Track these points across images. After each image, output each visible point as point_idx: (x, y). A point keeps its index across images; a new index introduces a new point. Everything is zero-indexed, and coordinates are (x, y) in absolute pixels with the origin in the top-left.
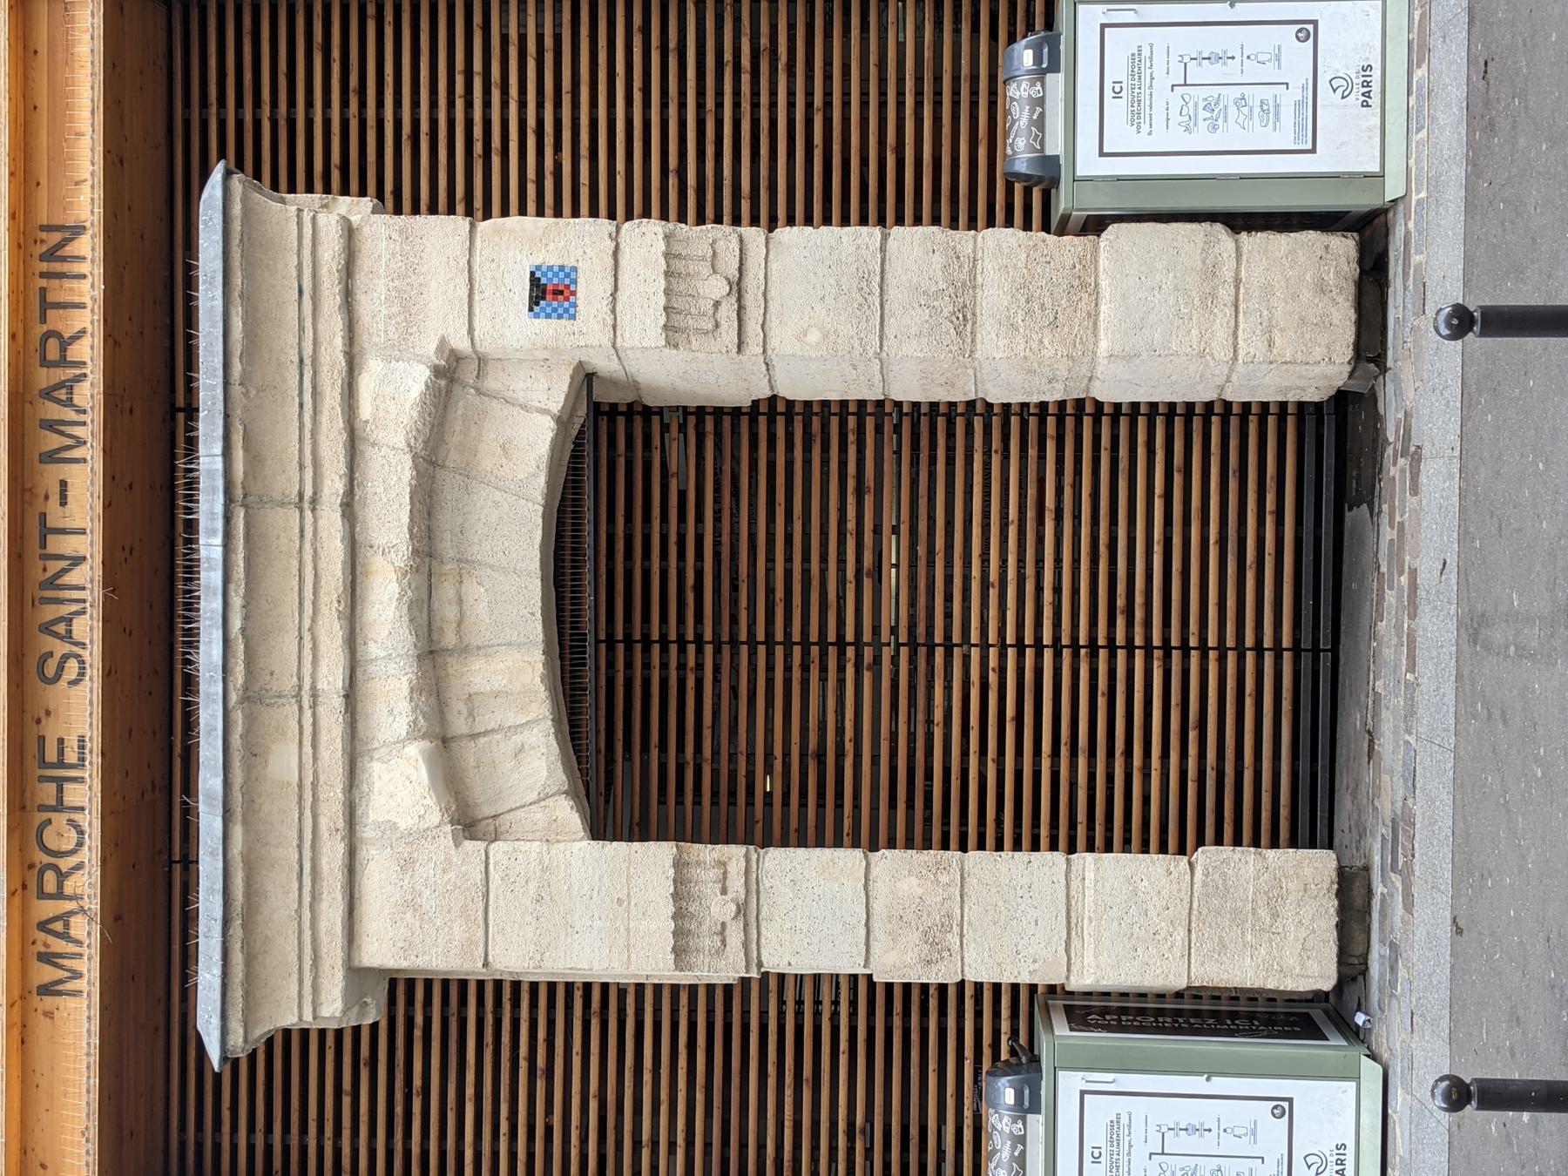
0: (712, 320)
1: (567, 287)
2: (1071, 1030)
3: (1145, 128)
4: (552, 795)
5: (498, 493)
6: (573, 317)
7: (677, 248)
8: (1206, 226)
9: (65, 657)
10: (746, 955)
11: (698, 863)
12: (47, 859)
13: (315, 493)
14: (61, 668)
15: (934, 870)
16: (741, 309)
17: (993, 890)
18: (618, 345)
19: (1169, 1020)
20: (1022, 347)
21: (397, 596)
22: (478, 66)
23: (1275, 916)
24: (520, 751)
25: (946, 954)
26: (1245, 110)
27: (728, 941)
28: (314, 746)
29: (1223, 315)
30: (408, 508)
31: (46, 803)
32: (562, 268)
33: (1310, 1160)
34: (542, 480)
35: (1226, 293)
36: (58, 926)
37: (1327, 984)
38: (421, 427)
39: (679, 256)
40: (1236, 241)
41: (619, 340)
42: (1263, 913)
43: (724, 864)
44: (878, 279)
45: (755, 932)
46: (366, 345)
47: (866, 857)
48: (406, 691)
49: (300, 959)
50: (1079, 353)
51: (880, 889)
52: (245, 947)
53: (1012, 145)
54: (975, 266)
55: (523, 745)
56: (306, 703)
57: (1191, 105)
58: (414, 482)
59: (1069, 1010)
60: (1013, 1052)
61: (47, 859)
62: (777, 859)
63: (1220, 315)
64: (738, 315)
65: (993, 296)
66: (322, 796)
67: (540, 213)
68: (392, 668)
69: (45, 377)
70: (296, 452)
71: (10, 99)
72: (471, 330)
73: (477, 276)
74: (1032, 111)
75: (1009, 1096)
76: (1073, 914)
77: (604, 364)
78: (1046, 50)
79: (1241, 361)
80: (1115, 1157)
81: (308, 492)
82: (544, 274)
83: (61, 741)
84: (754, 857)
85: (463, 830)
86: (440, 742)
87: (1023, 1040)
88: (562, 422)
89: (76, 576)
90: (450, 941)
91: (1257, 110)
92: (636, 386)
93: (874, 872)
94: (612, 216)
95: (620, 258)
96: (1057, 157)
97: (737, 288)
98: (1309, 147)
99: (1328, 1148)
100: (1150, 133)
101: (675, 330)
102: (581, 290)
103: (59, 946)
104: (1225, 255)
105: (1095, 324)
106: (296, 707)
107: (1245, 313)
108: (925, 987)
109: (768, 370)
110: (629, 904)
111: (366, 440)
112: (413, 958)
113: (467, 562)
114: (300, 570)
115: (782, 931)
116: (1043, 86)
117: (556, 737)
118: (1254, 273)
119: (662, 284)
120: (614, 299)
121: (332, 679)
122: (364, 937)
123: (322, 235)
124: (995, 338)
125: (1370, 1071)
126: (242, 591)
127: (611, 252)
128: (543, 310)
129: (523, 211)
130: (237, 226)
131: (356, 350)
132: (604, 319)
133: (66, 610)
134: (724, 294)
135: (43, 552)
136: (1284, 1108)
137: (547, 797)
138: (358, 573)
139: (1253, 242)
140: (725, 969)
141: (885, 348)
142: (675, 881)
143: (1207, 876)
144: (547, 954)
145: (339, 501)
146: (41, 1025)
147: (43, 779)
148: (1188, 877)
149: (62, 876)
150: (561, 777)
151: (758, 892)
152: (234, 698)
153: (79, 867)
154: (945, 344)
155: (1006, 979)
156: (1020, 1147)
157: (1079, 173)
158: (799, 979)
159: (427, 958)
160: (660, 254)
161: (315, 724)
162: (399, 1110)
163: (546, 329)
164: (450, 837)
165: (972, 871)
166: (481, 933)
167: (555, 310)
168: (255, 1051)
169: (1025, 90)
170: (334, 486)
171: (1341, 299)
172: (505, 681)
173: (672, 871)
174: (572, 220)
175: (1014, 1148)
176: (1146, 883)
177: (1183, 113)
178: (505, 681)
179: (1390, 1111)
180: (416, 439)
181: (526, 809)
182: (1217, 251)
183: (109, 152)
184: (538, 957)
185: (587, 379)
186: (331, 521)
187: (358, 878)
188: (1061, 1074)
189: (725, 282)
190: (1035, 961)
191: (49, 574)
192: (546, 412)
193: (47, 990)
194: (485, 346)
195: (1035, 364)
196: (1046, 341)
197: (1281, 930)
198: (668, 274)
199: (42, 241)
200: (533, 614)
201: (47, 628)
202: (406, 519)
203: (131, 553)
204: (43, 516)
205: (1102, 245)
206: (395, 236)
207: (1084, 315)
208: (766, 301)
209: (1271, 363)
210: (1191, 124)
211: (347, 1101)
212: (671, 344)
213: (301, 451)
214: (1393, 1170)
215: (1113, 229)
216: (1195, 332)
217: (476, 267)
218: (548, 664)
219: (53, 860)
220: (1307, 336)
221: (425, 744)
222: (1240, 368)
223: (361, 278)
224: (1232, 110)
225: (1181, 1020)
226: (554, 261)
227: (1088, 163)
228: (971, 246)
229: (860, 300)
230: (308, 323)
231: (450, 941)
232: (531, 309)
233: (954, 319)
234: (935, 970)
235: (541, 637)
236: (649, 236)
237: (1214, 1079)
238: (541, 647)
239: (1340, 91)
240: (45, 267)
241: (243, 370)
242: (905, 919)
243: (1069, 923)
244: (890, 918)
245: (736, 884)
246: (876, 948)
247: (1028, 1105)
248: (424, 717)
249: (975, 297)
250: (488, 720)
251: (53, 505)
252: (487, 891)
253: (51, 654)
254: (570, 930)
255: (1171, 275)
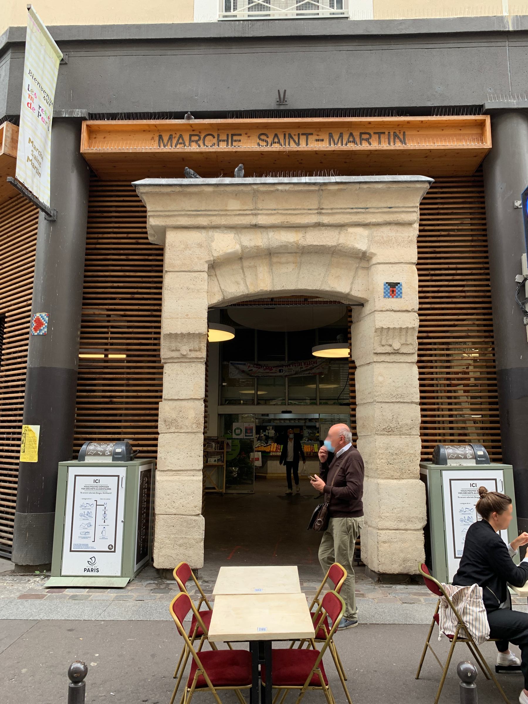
0: (385, 344)
1: (395, 295)
2: (141, 472)
3: (460, 495)
4: (223, 294)
5: (323, 275)
6: (385, 297)
7: (410, 332)
8: (426, 518)
9: (267, 142)
10: (169, 358)
11: (200, 342)
12: (202, 137)
13: (323, 213)
14: (263, 140)
15: (197, 422)
16: (389, 354)
17: (190, 444)
18: (376, 312)
19: (145, 506)
20: (380, 452)
21: (289, 241)
22: (459, 272)
23: (180, 546)
24: (238, 283)
25: (168, 427)
26: (86, 527)
27: (174, 352)
28: (239, 215)
29: (394, 525)
30: (318, 244)
31: (220, 137)
32: (401, 293)
33: (93, 559)
34: (328, 289)
35: (402, 525)
36: (181, 141)
37: (156, 565)
38: (346, 248)
39: (407, 332)
40: (421, 529)
41: (378, 313)
42: (181, 541)
43: (200, 350)
44: (402, 401)
45: (177, 361)
46: (373, 230)
47: (202, 399)
48: (257, 245)
49: (169, 211)
50: (379, 473)
51: (191, 404)
52: (173, 192)
53: (449, 448)
54: (407, 435)
55: (239, 284)
56: (253, 212)
57: (90, 507)
58: (327, 246)
59: (149, 471)
60: (135, 451)
61: (202, 137)
62: (203, 367)
63: (394, 523)
64: (387, 353)
65: (397, 442)
66: (222, 217)
67: (420, 286)
68: (265, 240)
69: (356, 134)
70: (337, 207)
71: (446, 121)
72: (379, 263)
73: (397, 265)
74: (462, 455)
75: (119, 450)
76: (181, 472)
77: (367, 309)
78: (484, 459)
79: (378, 531)
80: (96, 488)
81: (323, 211)
82: (399, 287)
83: (240, 141)
84: (202, 360)
85: (211, 264)
86: (241, 257)
87: (139, 455)
88: (347, 296)
89: (293, 144)
90: (174, 260)
91: (86, 531)
92: (359, 321)
93: (197, 402)
94: (420, 309)
95: (405, 312)
96: (447, 464)
97: (396, 352)
98: (72, 549)
99: (97, 566)
100: (459, 497)
101: (381, 332)
102: (394, 300)
103: (175, 141)
104: (415, 525)
105: (389, 478)
106: (252, 208)
107: (395, 533)
108: (157, 421)
109: (367, 364)
110: (187, 318)
111: (341, 230)
112: (169, 248)
113: (300, 265)
114: (297, 209)
115: (177, 370)
116: (471, 458)
117: (242, 295)
118: (409, 535)
119: (397, 326)
120: (391, 311)
121: (262, 220)
122: (176, 232)
123: (409, 214)
124: (383, 442)
125: (123, 582)
126: (291, 189)
127: (407, 309)
128: (387, 287)
129: (420, 281)
130: (412, 185)
131: (371, 226)
132: (384, 307)
133: (282, 141)
134: (394, 348)
135: (300, 134)
136: (112, 549)
137: (222, 292)
138: (297, 229)
139: (421, 536)
140: (164, 353)
141: (377, 404)
142: (194, 334)
143: (194, 521)
144: (169, 292)
145: (320, 221)
146: (150, 136)
147: (228, 135)
148: (194, 514)
149: (196, 142)
150: (229, 296)
151: (190, 362)
152: (255, 187)
153: (199, 146)
154: (380, 424)
155: (159, 449)
156: (101, 454)
157: (443, 472)
158: (161, 379)
159: (169, 252)
160: (407, 326)
161: (247, 215)
162: (122, 252)
163: (380, 288)
164: (209, 259)
165: (197, 436)
166: (177, 269)
167: (387, 291)
168: (139, 197)
169: (469, 452)
170: (326, 220)
171: (401, 568)
172: (261, 278)
173: (197, 332)
174: (418, 296)
175: (101, 451)
176: (192, 498)
177: (466, 509)
178: (261, 278)
179: (109, 590)
180: (342, 246)
181: (218, 285)
182: (417, 522)
183: (430, 151)
184: (169, 288)
185: (361, 304)
186: (314, 219)
187: (196, 230)
188: (125, 468)
189: (398, 348)
190: (165, 459)
191: (293, 136)
192: (351, 290)
193: (160, 137)
194: (373, 269)
195: (374, 457)
196: (382, 460)
197: (175, 548)
198: (401, 329)
199: (400, 133)
200: (283, 287)
201: (276, 135)
202: (315, 244)
203: (300, 163)
204: (312, 134)
205: (417, 480)
206: (410, 238)
207: (392, 474)
208: (392, 362)
209: (378, 542)
210: (463, 512)
211: (125, 235)
212: (376, 330)
213: (337, 209)
214: (88, 592)
215: (423, 484)
216: (388, 514)
217: (400, 265)
218: (266, 291)
219: (202, 139)
220: (387, 556)
221: (240, 251)
222: (375, 531)
223: (395, 228)
224: (87, 522)
225: (145, 510)
226: (403, 290)
227: (447, 475)
228: (414, 433)
229: (394, 395)
230: (380, 210)
231: (174, 260)
232: (387, 283)
233: (389, 428)
234: (162, 423)
235: (275, 289)
236: (413, 322)
237: (122, 524)
238: (272, 290)
239: (90, 560)
240: (392, 133)
241: (364, 189)
242: (180, 412)
243: (178, 471)
244: (181, 407)
245: (193, 355)
246: (170, 403)
247: (115, 456)
248: (249, 251)
249: (397, 435)
250: (248, 273)
251: (315, 137)
252: (191, 272)
253: (268, 137)
254: (178, 299)
255: (408, 505)
